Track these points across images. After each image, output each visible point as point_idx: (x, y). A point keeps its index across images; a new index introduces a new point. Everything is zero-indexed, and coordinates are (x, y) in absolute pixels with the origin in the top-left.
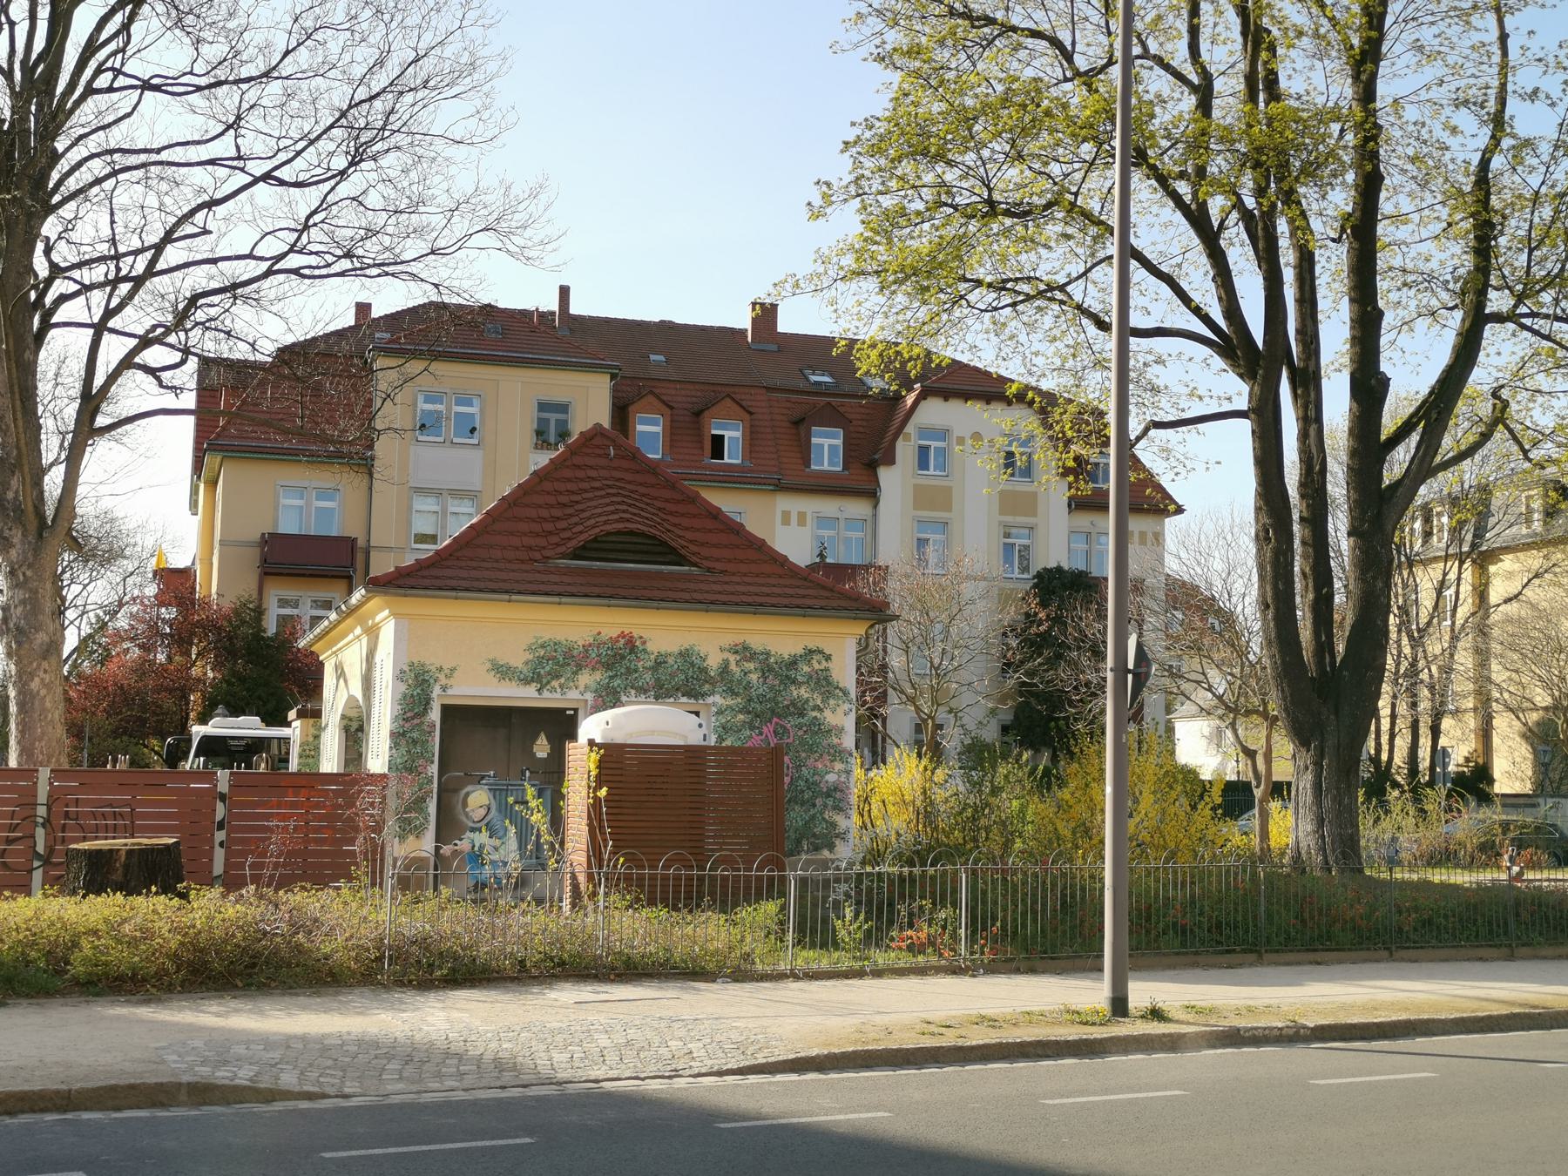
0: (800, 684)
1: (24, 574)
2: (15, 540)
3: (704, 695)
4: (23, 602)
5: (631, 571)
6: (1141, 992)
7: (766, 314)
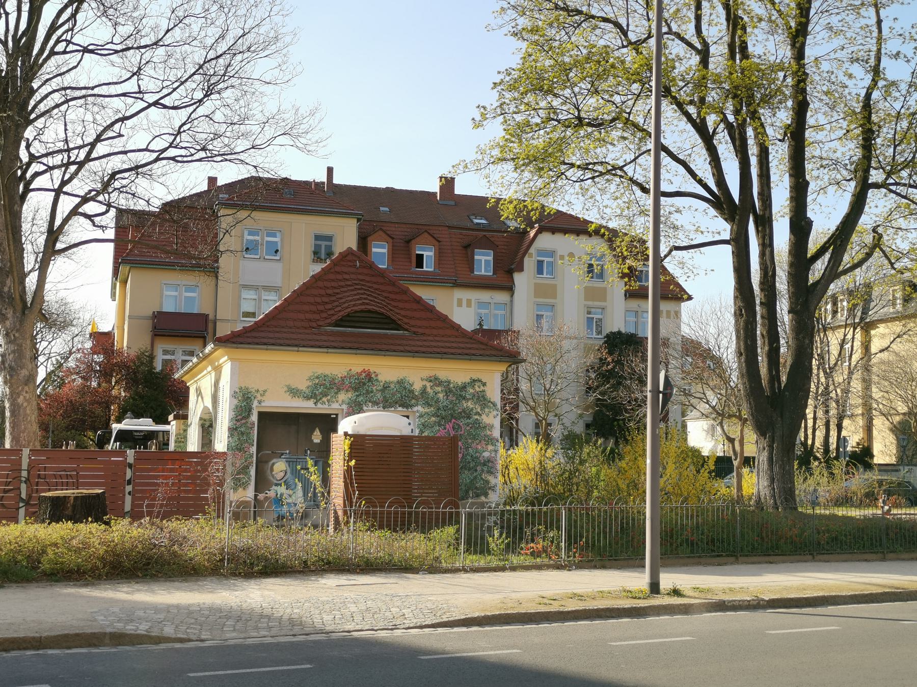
0: (468, 400)
1: (14, 335)
2: (9, 316)
3: (412, 406)
4: (14, 352)
5: (369, 334)
6: (667, 580)
7: (448, 184)
